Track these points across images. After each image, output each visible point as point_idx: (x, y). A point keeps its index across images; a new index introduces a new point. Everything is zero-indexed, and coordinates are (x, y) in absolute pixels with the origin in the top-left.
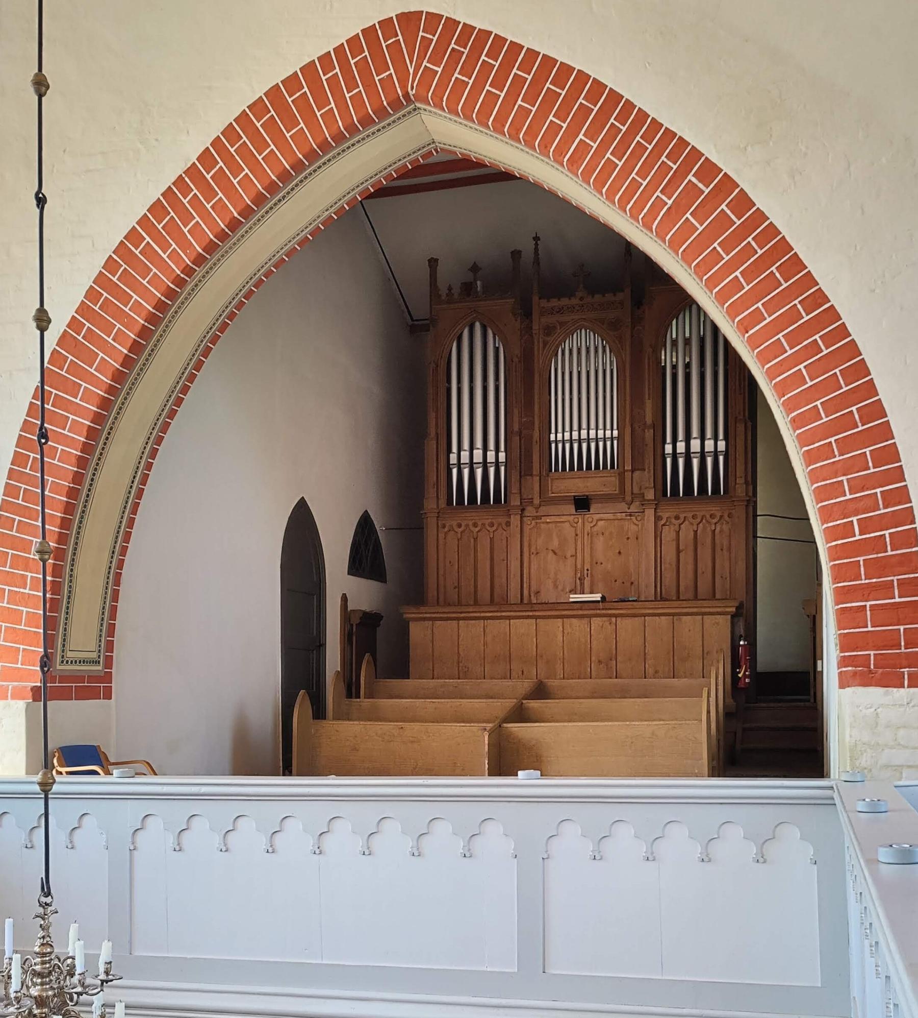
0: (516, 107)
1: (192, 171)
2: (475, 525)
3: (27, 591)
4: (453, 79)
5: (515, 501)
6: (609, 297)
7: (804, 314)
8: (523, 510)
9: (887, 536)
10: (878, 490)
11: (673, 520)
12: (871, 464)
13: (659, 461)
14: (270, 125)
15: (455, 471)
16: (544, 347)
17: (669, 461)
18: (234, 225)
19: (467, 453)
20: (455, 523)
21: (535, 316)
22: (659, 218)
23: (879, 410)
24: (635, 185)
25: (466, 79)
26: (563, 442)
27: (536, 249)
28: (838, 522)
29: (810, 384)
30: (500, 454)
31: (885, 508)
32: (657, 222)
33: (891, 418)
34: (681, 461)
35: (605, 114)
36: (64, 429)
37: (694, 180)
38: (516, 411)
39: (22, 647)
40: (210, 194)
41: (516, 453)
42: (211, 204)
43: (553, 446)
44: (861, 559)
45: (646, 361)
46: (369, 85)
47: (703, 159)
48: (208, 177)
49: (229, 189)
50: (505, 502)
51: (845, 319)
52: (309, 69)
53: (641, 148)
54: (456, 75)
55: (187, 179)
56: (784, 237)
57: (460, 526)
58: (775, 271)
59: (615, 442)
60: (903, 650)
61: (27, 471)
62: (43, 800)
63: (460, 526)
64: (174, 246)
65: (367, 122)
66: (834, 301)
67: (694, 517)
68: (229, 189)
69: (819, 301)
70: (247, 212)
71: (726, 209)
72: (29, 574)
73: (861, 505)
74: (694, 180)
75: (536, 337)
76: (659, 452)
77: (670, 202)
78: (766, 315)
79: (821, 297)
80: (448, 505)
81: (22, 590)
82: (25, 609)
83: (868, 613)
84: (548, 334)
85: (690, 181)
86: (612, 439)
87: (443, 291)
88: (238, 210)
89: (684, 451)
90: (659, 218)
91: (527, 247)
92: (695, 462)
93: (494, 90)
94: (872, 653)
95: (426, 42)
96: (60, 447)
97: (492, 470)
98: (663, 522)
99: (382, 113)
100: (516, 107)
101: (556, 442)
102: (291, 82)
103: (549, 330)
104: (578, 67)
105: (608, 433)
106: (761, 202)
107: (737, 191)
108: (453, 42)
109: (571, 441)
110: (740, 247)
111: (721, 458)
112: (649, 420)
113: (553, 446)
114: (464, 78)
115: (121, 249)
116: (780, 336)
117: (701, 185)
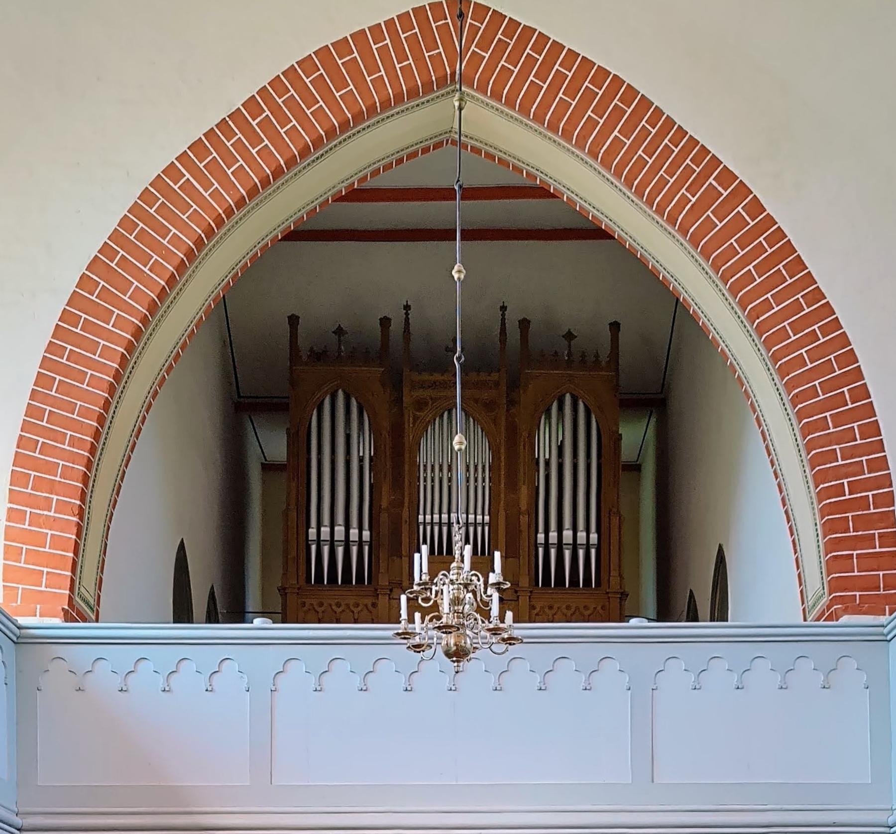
1: (235, 115)
2: (338, 605)
3: (52, 514)
4: (500, 66)
5: (383, 581)
6: (483, 376)
7: (805, 307)
8: (391, 590)
9: (871, 497)
11: (547, 610)
16: (414, 423)
17: (541, 550)
20: (315, 602)
21: (406, 391)
22: (684, 212)
24: (663, 182)
25: (512, 68)
26: (440, 524)
27: (503, 319)
28: (833, 483)
29: (810, 366)
34: (553, 552)
35: (636, 116)
38: (385, 489)
39: (45, 570)
40: (255, 140)
41: (385, 530)
42: (257, 149)
43: (421, 528)
45: (522, 447)
46: (419, 59)
47: (722, 166)
49: (275, 137)
52: (360, 36)
53: (668, 150)
55: (230, 123)
57: (321, 605)
58: (782, 268)
59: (487, 528)
60: (882, 592)
61: (53, 393)
62: (336, 539)
63: (321, 605)
65: (413, 93)
66: (829, 298)
67: (568, 607)
68: (275, 137)
69: (818, 297)
70: (291, 162)
71: (741, 211)
72: (55, 497)
73: (850, 469)
75: (406, 411)
78: (774, 305)
81: (46, 513)
83: (855, 560)
84: (420, 409)
85: (711, 183)
87: (304, 354)
88: (285, 158)
89: (556, 542)
90: (684, 212)
93: (537, 81)
94: (858, 594)
95: (474, 30)
97: (354, 550)
98: (535, 612)
99: (428, 87)
101: (425, 523)
102: (342, 46)
103: (420, 405)
104: (613, 72)
108: (500, 32)
109: (432, 524)
110: (752, 245)
111: (593, 551)
112: (524, 506)
113: (421, 528)
114: (510, 66)
115: (157, 182)
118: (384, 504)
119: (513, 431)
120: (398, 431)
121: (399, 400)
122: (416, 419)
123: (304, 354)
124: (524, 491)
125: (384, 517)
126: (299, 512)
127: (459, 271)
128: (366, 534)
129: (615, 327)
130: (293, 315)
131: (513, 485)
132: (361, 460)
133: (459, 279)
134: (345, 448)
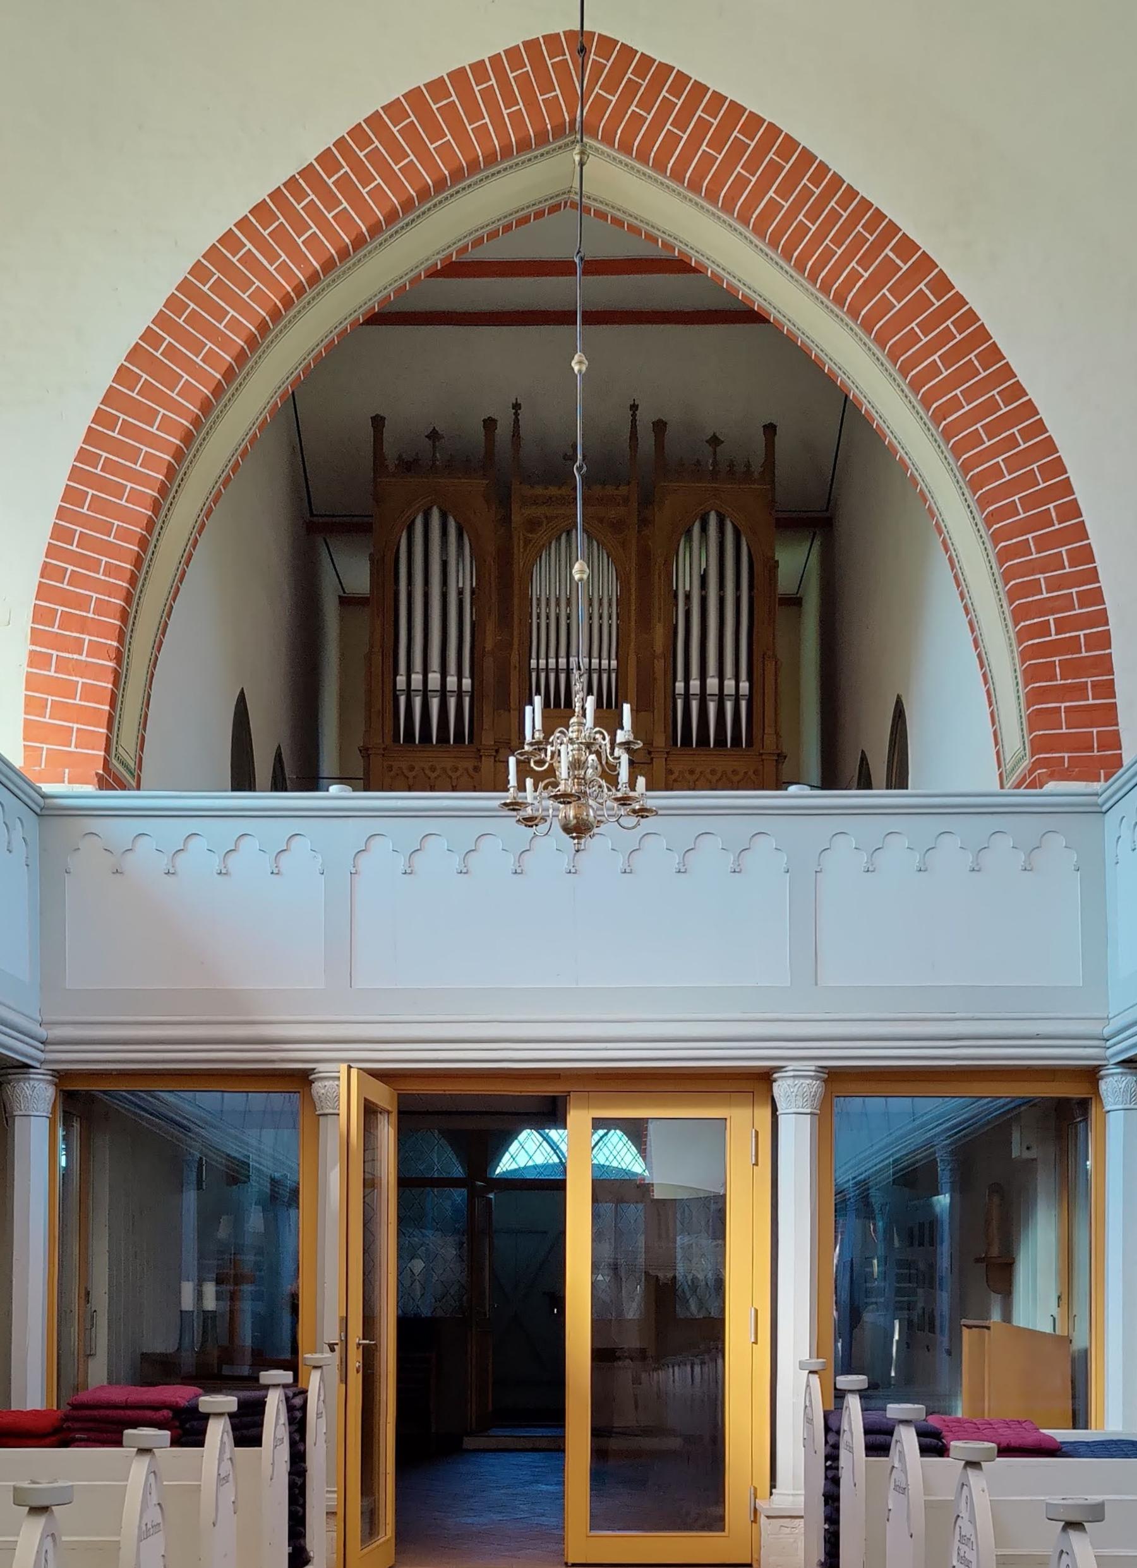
0: (700, 152)
1: (308, 172)
3: (83, 658)
4: (630, 112)
5: (487, 739)
8: (497, 751)
10: (1074, 590)
11: (687, 775)
12: (1066, 563)
13: (670, 700)
14: (409, 132)
15: (402, 699)
17: (680, 702)
18: (359, 242)
19: (420, 677)
21: (515, 507)
23: (1073, 510)
24: (828, 254)
26: (547, 670)
30: (464, 681)
31: (1080, 608)
32: (852, 294)
33: (1085, 517)
34: (694, 705)
36: (135, 464)
37: (891, 254)
39: (76, 726)
40: (331, 202)
43: (534, 675)
44: (1056, 659)
46: (531, 104)
48: (330, 182)
50: (471, 741)
51: (1043, 414)
54: (633, 108)
55: (301, 181)
56: (982, 324)
57: (412, 768)
62: (430, 688)
63: (412, 768)
64: (284, 257)
65: (524, 145)
66: (1031, 395)
67: (713, 772)
70: (375, 229)
71: (924, 288)
72: (87, 638)
74: (891, 254)
76: (670, 691)
77: (866, 275)
79: (1018, 390)
80: (394, 741)
82: (81, 680)
84: (532, 531)
86: (609, 671)
87: (391, 464)
91: (503, 430)
92: (712, 707)
93: (675, 130)
94: (1066, 755)
96: (130, 485)
98: (673, 777)
100: (700, 152)
102: (437, 87)
103: (533, 525)
104: (768, 120)
105: (605, 662)
106: (960, 285)
107: (936, 271)
108: (630, 71)
109: (547, 670)
112: (659, 646)
113: (534, 675)
115: (212, 253)
116: (978, 425)
117: (898, 262)
118: (489, 645)
119: (645, 556)
120: (505, 556)
121: (506, 519)
122: (527, 542)
123: (391, 464)
124: (659, 632)
125: (489, 663)
126: (386, 655)
127: (580, 362)
128: (467, 683)
129: (770, 430)
130: (377, 415)
131: (645, 622)
132: (460, 592)
133: (580, 371)
134: (442, 576)
